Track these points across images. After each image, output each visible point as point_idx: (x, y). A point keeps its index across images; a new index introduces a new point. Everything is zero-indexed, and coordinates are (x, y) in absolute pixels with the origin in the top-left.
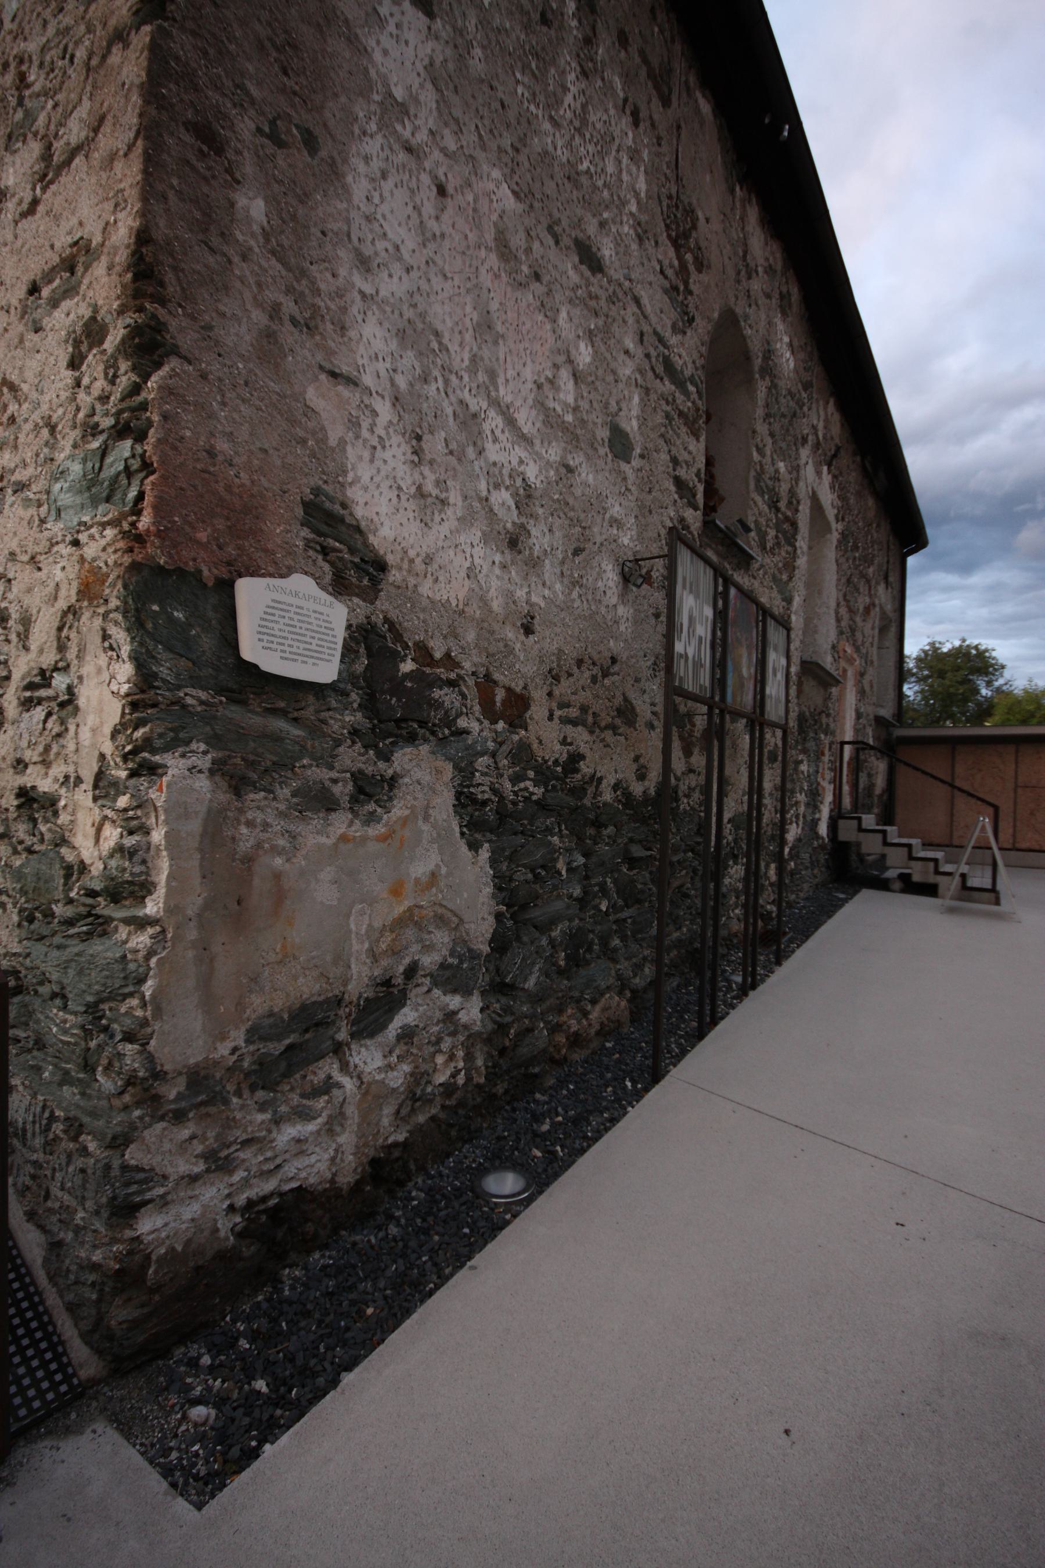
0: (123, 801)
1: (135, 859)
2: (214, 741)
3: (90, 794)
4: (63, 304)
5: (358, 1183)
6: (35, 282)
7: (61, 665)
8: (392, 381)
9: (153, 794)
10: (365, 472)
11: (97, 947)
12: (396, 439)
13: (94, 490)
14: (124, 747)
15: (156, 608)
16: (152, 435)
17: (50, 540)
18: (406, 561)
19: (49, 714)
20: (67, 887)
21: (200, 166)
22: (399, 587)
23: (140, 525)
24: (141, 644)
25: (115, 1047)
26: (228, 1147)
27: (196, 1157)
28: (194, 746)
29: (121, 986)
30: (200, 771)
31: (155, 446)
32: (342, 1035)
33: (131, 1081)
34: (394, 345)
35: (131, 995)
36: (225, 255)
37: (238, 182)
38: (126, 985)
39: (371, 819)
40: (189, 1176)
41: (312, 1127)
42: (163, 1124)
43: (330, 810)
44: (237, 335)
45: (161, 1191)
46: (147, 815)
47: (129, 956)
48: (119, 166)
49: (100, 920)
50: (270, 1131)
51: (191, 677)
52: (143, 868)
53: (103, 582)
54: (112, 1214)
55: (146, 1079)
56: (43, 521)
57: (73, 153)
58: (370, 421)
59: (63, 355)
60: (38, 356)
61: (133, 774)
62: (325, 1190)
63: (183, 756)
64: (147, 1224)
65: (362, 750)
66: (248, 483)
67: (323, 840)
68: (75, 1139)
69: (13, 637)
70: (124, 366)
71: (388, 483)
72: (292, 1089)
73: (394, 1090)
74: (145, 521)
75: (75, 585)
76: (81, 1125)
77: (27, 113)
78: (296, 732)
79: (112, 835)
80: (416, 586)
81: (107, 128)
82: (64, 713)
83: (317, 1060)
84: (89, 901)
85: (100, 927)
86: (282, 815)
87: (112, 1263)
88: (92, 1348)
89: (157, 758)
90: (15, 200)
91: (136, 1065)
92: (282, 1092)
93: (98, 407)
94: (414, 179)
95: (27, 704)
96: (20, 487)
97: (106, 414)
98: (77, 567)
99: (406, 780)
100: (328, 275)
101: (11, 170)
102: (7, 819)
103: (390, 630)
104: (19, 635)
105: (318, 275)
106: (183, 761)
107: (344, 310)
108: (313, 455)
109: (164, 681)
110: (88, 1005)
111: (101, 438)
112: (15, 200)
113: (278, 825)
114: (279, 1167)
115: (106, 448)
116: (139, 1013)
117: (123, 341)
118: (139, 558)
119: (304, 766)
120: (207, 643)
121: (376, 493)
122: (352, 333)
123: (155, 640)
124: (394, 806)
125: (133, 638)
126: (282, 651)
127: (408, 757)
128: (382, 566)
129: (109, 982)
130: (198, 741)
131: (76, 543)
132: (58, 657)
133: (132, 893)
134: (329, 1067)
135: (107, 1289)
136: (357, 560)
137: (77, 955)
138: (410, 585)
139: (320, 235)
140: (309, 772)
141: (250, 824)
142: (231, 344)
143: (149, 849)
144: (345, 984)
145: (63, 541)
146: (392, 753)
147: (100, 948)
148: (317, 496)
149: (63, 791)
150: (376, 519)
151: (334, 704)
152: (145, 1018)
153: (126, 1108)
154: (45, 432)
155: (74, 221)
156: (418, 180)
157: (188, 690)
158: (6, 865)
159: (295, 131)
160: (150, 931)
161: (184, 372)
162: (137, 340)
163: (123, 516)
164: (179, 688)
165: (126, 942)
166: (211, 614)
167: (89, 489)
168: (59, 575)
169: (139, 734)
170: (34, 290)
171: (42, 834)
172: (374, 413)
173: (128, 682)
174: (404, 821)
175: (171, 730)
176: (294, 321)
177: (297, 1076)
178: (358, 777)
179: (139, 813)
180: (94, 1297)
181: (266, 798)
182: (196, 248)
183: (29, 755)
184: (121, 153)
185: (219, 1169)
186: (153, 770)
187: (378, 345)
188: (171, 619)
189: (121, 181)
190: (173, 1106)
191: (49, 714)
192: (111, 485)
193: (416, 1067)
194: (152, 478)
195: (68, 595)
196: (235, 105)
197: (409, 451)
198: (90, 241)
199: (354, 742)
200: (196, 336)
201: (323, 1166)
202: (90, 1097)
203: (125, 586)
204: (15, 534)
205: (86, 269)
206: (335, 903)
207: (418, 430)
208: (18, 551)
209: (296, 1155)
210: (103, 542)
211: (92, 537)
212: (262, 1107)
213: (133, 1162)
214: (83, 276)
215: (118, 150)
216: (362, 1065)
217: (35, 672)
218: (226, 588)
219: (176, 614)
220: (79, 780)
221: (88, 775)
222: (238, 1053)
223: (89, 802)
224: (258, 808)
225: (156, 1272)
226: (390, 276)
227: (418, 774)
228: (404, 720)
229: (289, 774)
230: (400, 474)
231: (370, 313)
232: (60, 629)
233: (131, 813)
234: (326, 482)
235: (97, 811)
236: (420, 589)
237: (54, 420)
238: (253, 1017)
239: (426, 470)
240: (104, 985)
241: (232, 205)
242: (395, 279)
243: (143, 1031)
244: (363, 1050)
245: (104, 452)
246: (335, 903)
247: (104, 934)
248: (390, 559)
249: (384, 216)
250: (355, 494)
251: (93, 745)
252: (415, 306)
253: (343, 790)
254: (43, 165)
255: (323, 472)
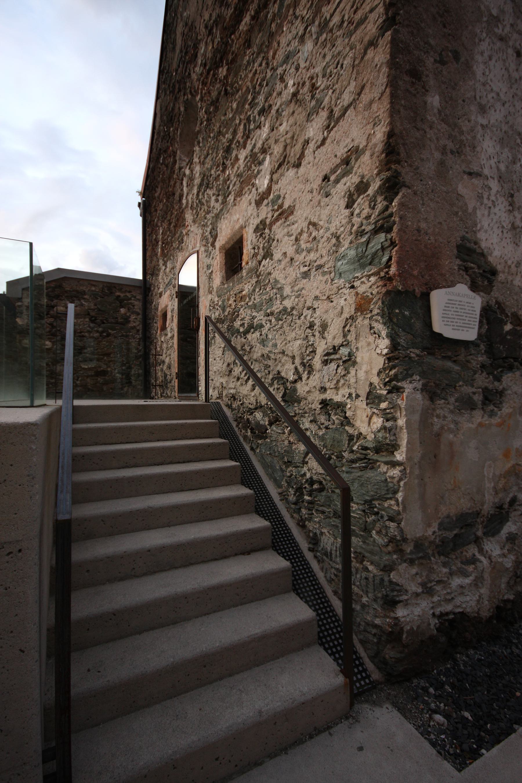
0: (383, 405)
1: (392, 433)
2: (423, 374)
3: (365, 402)
4: (342, 180)
5: (491, 617)
6: (326, 175)
7: (344, 343)
8: (498, 169)
9: (399, 402)
10: (485, 223)
11: (370, 474)
12: (501, 199)
13: (361, 261)
14: (385, 379)
15: (397, 311)
16: (395, 228)
17: (338, 288)
18: (507, 268)
19: (338, 366)
20: (350, 446)
21: (412, 90)
22: (503, 283)
23: (391, 273)
24: (392, 329)
25: (384, 523)
26: (431, 582)
27: (418, 584)
28: (414, 377)
29: (385, 494)
30: (418, 390)
31: (397, 233)
32: (480, 533)
33: (392, 540)
34: (498, 148)
35: (391, 499)
36: (423, 130)
37: (427, 91)
38: (388, 494)
39: (492, 414)
40: (416, 593)
41: (467, 581)
42: (405, 565)
43: (472, 409)
44: (429, 168)
45: (406, 597)
46: (396, 412)
47: (389, 480)
48: (375, 107)
49: (371, 461)
50: (448, 578)
51: (412, 343)
52: (394, 438)
53: (370, 302)
54: (385, 603)
55: (399, 541)
56: (332, 280)
57: (346, 110)
58: (488, 193)
59: (343, 203)
60: (328, 207)
61: (390, 392)
62: (475, 617)
63: (410, 382)
64: (401, 612)
65: (487, 376)
66: (434, 241)
67: (471, 425)
68: (361, 562)
69: (317, 334)
70: (379, 199)
71: (497, 226)
72: (456, 558)
73: (507, 569)
74: (393, 270)
75: (353, 306)
76: (364, 556)
77: (317, 101)
78: (457, 368)
79: (378, 422)
80: (512, 281)
81: (367, 90)
82: (346, 365)
83: (468, 545)
84: (364, 452)
85: (371, 465)
86: (452, 412)
87: (387, 627)
88: (375, 665)
89: (399, 384)
90: (313, 142)
91: (396, 533)
92: (452, 559)
93: (365, 222)
94: (505, 53)
95: (326, 363)
96: (320, 267)
97: (369, 224)
98: (354, 298)
99: (509, 392)
100: (466, 122)
101: (311, 129)
102: (315, 414)
103: (498, 308)
104: (319, 332)
105: (462, 124)
106: (411, 385)
107: (474, 138)
108: (461, 220)
109: (403, 346)
110: (366, 501)
111: (367, 236)
112: (313, 142)
113: (450, 417)
114: (453, 598)
115: (369, 240)
116: (395, 508)
117: (380, 187)
118: (390, 288)
119: (460, 386)
120: (418, 325)
121: (491, 233)
122: (478, 149)
123: (398, 327)
124: (503, 407)
125: (388, 327)
126: (453, 326)
127: (510, 378)
128: (494, 272)
129: (379, 492)
130: (416, 375)
131: (353, 287)
132: (344, 340)
133: (387, 450)
134: (472, 550)
135: (383, 639)
136: (481, 271)
137: (359, 476)
138: (509, 280)
139: (462, 103)
140: (463, 389)
141: (438, 416)
142: (426, 173)
143: (396, 428)
144: (483, 505)
145: (344, 287)
146: (501, 376)
147: (372, 475)
148: (463, 241)
149: (348, 401)
150: (491, 247)
151: (473, 352)
152: (399, 511)
153: (389, 553)
154: (334, 241)
155: (349, 140)
156: (507, 53)
157: (411, 350)
158: (315, 434)
159: (450, 54)
160: (398, 468)
161: (408, 193)
162: (387, 185)
163: (381, 270)
164: (407, 349)
165: (386, 473)
166: (419, 311)
167: (359, 261)
168: (342, 302)
169: (393, 372)
170: (326, 178)
171: (334, 421)
172: (490, 189)
173: (386, 348)
174: (510, 415)
175: (405, 370)
176: (452, 152)
177: (459, 551)
178: (485, 390)
179: (392, 411)
180: (375, 640)
181: (445, 403)
182: (412, 131)
183: (328, 385)
184: (377, 98)
185: (427, 593)
186: (398, 390)
187: (491, 151)
188: (404, 316)
189: (377, 112)
190: (410, 556)
191: (338, 366)
192: (372, 256)
193: (517, 558)
194: (395, 249)
195: (349, 311)
196: (425, 53)
197: (508, 204)
198: (359, 146)
199: (482, 372)
200: (412, 174)
201: (473, 604)
202: (368, 544)
203: (383, 303)
204: (318, 288)
205: (356, 160)
206: (477, 460)
207: (512, 192)
208: (320, 295)
209: (460, 594)
210: (370, 284)
211: (363, 283)
212: (445, 565)
213: (394, 580)
214: (355, 164)
215: (374, 98)
216: (490, 551)
217: (331, 348)
218: (426, 297)
219: (406, 313)
220: (358, 396)
221: (363, 393)
222: (435, 535)
223: (365, 406)
224: (441, 408)
225: (406, 638)
226: (495, 111)
227: (515, 388)
228: (506, 358)
229: (453, 390)
230: (503, 219)
231: (486, 135)
232: (344, 327)
233: (388, 411)
234: (467, 233)
235: (369, 410)
236: (514, 282)
237: (338, 234)
238: (442, 517)
239: (516, 213)
240: (376, 492)
241: (426, 103)
242: (498, 111)
243: (398, 517)
244: (489, 543)
245: (368, 242)
246: (477, 460)
247: (372, 468)
248: (499, 268)
249: (491, 80)
250: (481, 236)
251: (366, 379)
252: (507, 123)
253: (478, 398)
254: (328, 121)
255: (466, 228)
